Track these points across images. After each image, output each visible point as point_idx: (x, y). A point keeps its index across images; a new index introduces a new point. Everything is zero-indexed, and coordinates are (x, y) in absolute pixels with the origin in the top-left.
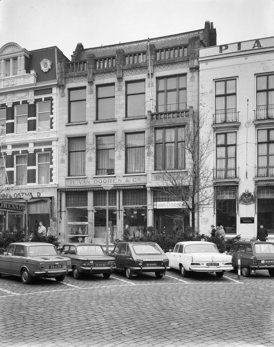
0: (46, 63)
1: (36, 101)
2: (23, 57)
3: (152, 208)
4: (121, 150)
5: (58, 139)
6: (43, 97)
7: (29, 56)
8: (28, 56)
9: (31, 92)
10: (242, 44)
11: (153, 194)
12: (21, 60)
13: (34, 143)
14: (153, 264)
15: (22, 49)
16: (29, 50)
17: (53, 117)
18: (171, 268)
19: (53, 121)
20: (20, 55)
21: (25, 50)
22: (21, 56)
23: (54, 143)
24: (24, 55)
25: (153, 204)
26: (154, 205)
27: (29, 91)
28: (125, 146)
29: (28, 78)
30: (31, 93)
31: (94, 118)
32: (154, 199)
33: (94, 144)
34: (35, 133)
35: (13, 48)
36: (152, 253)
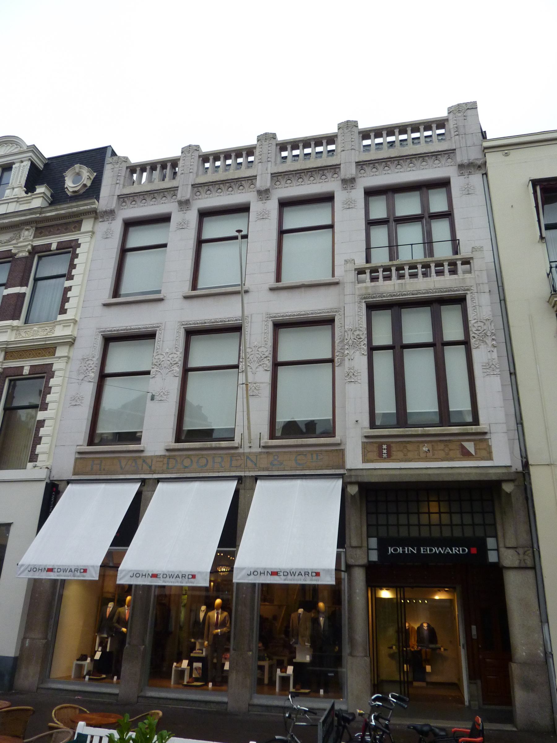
0: (78, 174)
1: (34, 251)
2: (27, 164)
3: (364, 561)
4: (261, 369)
5: (74, 340)
6: (54, 241)
7: (43, 167)
8: (41, 166)
9: (27, 230)
10: (550, 261)
11: (364, 509)
12: (19, 169)
13: (6, 353)
14: (404, 548)
15: (27, 146)
16: (47, 157)
17: (71, 287)
18: (60, 325)
19: (69, 294)
20: (20, 160)
21: (34, 149)
22: (22, 162)
23: (61, 352)
24: (30, 159)
25: (365, 544)
26: (369, 549)
27: (22, 229)
28: (271, 356)
29: (27, 203)
30: (26, 233)
31: (186, 289)
32: (368, 526)
33: (177, 351)
34: (13, 327)
35: (9, 147)
36: (539, 464)
